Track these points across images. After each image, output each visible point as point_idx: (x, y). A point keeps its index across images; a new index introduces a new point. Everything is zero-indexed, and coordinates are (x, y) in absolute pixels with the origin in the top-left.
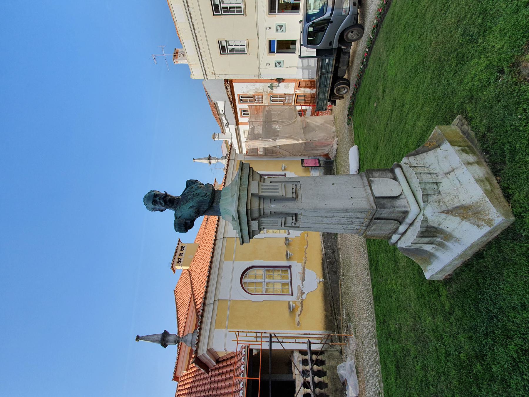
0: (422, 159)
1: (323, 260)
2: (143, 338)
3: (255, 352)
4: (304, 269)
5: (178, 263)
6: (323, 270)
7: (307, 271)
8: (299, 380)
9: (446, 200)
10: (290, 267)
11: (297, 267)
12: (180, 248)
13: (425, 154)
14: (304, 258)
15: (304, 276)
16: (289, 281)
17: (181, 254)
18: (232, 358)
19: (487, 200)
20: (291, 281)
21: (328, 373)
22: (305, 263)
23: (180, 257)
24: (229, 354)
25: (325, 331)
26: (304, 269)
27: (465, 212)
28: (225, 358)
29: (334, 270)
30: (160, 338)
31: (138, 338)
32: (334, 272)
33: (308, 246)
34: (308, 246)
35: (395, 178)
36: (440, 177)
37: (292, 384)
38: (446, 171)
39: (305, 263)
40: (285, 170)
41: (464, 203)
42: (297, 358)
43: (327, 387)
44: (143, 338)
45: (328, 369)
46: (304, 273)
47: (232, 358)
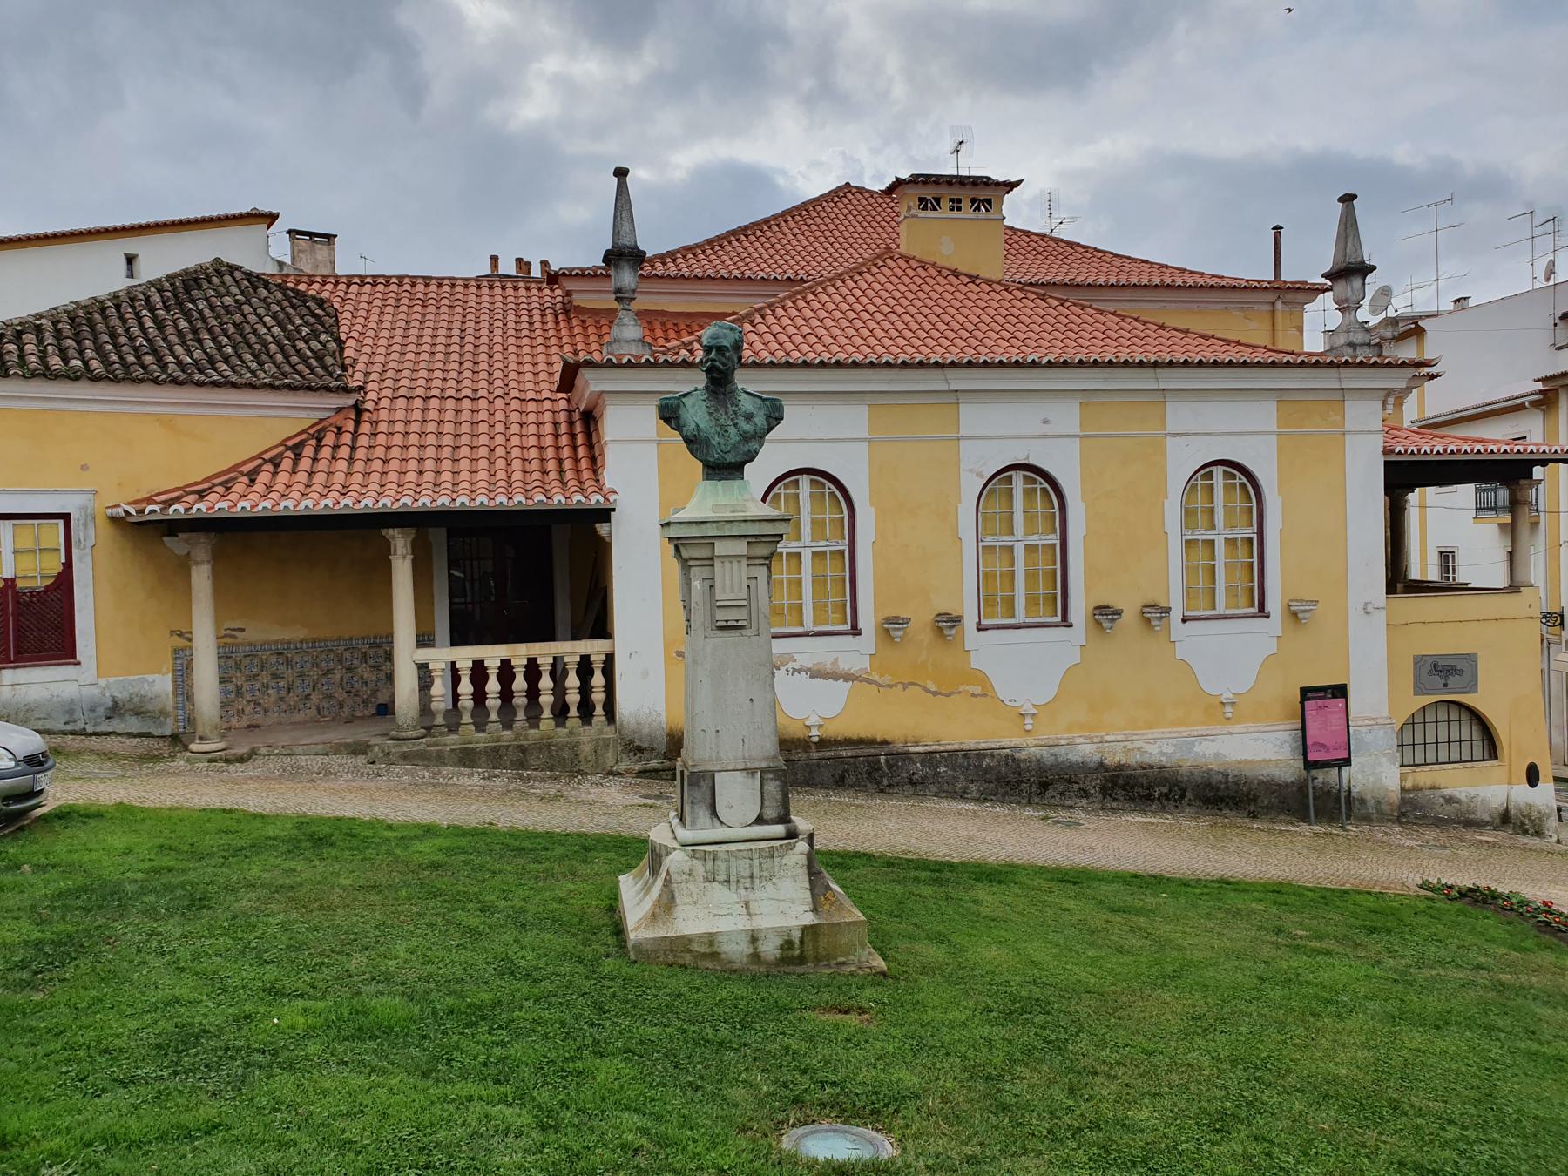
0: (794, 878)
1: (885, 743)
2: (622, 189)
3: (602, 529)
4: (848, 677)
5: (921, 200)
6: (848, 742)
7: (843, 687)
8: (544, 652)
9: (691, 886)
10: (855, 631)
11: (855, 654)
12: (982, 194)
13: (807, 885)
14: (887, 679)
15: (826, 676)
16: (809, 625)
17: (956, 204)
18: (593, 459)
19: (670, 935)
20: (806, 634)
21: (562, 731)
22: (870, 682)
23: (945, 204)
24: (602, 454)
25: (666, 731)
26: (848, 677)
27: (666, 905)
28: (594, 440)
29: (851, 779)
30: (625, 241)
31: (621, 173)
32: (842, 778)
33: (935, 694)
34: (935, 694)
35: (760, 820)
36: (743, 892)
37: (551, 637)
38: (752, 905)
39: (870, 682)
40: (1294, 616)
41: (680, 908)
42: (595, 648)
43: (531, 727)
44: (622, 189)
45: (571, 733)
46: (835, 676)
47: (593, 459)
